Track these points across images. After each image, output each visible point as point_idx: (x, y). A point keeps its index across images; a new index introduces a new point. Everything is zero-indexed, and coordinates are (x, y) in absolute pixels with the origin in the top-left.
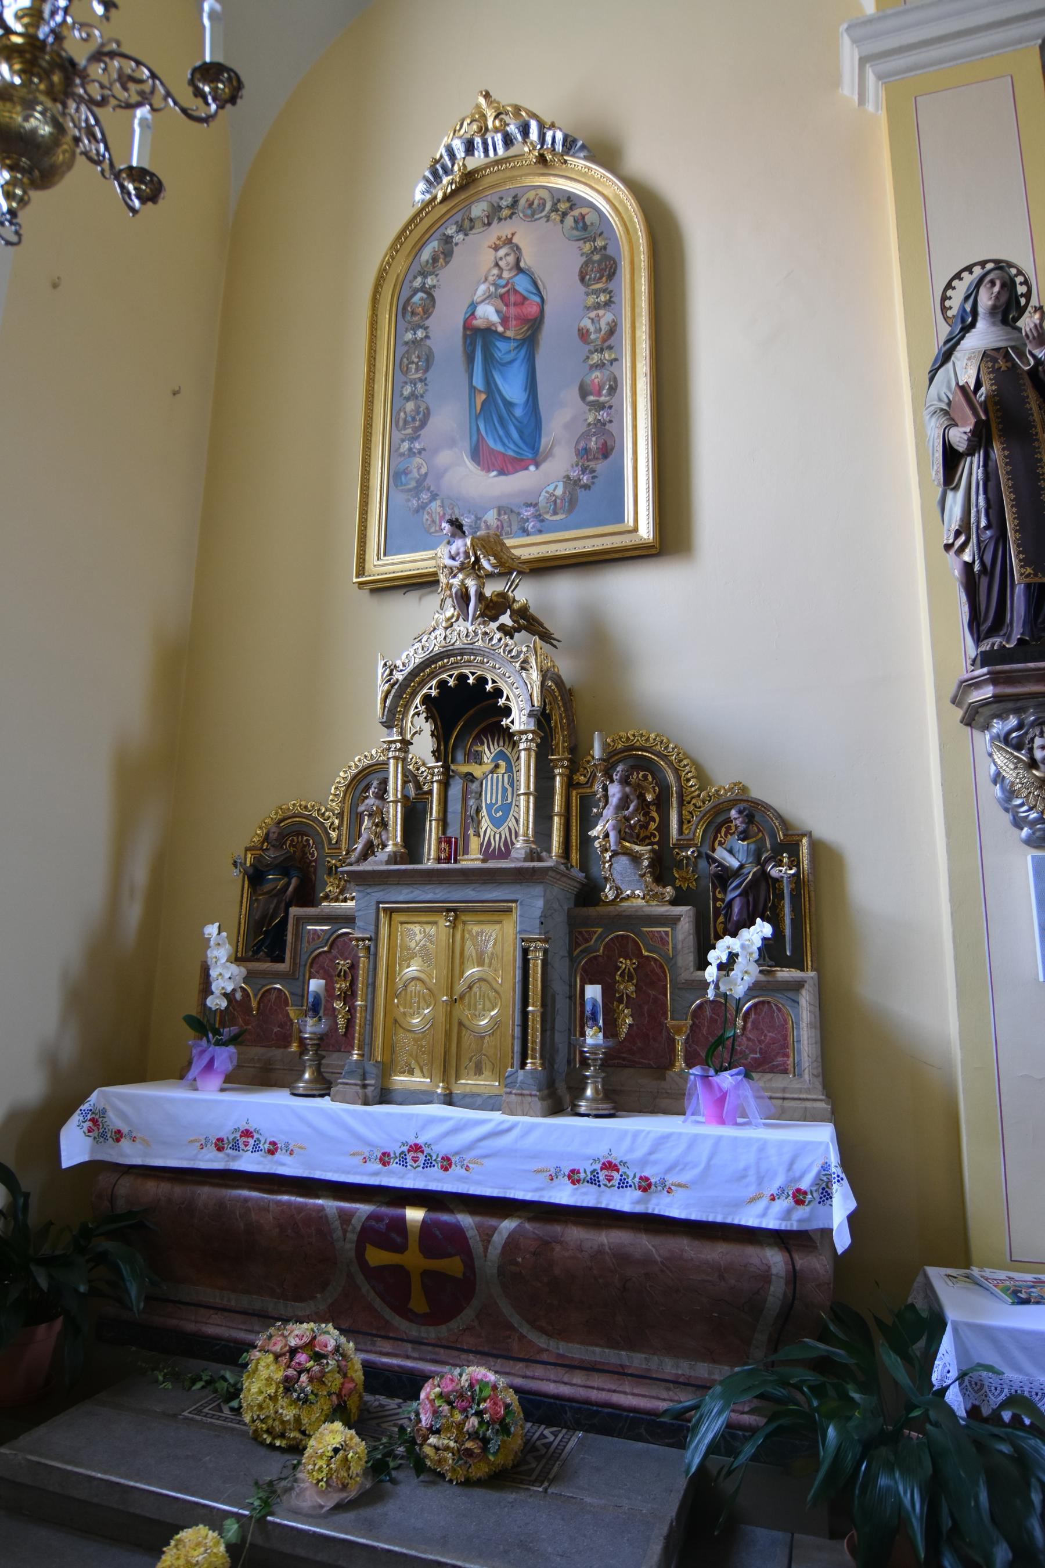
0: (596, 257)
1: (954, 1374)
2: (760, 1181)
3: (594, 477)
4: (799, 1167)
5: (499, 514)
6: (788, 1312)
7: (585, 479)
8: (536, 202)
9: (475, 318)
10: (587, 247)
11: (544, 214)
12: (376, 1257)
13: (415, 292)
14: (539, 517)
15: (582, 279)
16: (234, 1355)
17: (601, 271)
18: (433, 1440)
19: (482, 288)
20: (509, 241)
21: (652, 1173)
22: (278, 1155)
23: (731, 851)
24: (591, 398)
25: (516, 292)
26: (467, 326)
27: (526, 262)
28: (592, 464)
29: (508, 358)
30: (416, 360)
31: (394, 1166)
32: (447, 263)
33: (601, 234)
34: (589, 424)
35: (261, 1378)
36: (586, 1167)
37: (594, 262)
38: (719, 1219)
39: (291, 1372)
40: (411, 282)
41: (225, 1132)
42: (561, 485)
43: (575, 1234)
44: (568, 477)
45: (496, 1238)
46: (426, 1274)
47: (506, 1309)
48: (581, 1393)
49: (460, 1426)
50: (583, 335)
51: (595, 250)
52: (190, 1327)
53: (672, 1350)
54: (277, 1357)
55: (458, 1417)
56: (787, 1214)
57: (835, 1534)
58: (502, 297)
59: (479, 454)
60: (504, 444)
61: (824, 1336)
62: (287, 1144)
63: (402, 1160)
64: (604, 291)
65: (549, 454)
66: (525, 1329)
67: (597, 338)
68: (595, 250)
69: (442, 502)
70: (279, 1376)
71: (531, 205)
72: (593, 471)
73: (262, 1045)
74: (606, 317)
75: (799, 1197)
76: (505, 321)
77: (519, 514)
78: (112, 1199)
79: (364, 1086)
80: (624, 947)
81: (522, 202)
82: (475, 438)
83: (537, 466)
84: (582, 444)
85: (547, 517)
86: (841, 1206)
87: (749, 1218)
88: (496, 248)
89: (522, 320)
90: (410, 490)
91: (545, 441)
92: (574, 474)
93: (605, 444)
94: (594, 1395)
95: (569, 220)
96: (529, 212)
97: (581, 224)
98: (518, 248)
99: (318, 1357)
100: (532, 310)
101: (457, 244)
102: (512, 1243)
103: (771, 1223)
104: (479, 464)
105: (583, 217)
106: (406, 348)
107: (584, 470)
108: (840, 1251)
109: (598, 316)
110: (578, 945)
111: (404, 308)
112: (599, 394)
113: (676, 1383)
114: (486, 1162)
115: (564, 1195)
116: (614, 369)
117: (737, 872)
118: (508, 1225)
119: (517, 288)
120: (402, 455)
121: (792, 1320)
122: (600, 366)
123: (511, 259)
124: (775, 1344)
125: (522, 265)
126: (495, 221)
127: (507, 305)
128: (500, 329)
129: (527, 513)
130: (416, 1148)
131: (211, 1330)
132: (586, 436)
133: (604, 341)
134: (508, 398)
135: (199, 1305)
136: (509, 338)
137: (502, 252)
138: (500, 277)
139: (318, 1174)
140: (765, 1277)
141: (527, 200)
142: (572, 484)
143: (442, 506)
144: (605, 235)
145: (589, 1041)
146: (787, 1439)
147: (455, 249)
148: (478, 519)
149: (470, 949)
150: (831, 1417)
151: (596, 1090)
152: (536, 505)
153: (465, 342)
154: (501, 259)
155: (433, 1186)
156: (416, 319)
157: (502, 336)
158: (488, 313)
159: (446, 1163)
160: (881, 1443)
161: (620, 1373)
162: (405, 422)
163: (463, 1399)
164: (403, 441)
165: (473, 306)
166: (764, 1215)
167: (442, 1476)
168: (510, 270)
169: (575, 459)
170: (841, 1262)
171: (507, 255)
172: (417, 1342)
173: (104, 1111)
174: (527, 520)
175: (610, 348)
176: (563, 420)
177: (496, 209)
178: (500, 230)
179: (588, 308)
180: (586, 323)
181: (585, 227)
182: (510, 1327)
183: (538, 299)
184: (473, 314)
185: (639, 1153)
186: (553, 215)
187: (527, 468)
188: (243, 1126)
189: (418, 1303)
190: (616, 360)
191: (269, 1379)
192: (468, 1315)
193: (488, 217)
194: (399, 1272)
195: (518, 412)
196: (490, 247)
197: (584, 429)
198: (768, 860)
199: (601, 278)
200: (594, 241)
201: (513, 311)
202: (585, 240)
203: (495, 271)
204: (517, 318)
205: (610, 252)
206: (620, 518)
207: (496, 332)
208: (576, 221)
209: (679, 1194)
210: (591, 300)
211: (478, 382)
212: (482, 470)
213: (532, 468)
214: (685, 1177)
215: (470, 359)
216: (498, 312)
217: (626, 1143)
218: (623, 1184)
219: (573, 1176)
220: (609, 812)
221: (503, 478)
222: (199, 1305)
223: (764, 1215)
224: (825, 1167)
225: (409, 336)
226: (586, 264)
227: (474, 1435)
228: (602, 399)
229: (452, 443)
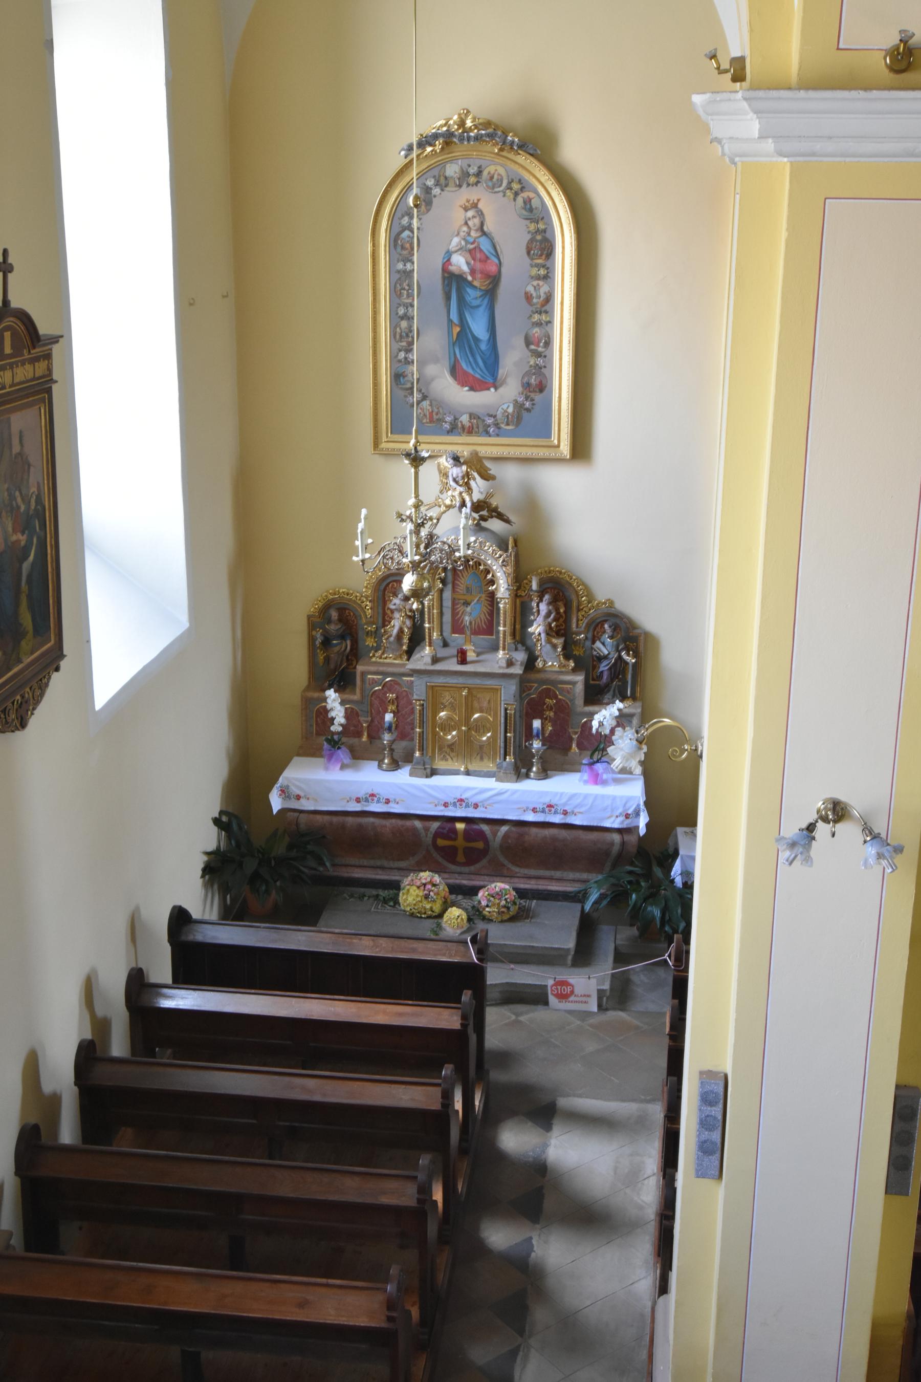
0: (539, 237)
1: (679, 872)
2: (612, 810)
3: (533, 404)
4: (628, 805)
5: (470, 418)
6: (620, 855)
7: (527, 404)
8: (496, 177)
9: (451, 264)
10: (532, 227)
11: (501, 189)
12: (441, 842)
13: (404, 229)
14: (497, 425)
15: (528, 253)
16: (396, 886)
17: (542, 250)
18: (487, 909)
19: (456, 240)
20: (475, 206)
21: (567, 808)
22: (391, 804)
23: (603, 644)
24: (533, 347)
25: (481, 250)
26: (445, 269)
27: (489, 226)
28: (532, 395)
29: (477, 302)
30: (407, 288)
31: (450, 807)
32: (428, 211)
33: (543, 218)
34: (531, 366)
35: (410, 897)
36: (540, 807)
37: (537, 241)
38: (595, 824)
39: (426, 892)
40: (400, 219)
41: (361, 794)
42: (511, 406)
43: (534, 830)
44: (516, 401)
45: (499, 834)
46: (465, 848)
47: (502, 859)
48: (535, 887)
49: (499, 904)
50: (528, 297)
51: (538, 231)
52: (346, 875)
53: (572, 869)
54: (418, 887)
55: (497, 901)
56: (622, 822)
57: (632, 925)
58: (470, 251)
59: (455, 371)
60: (473, 369)
61: (632, 864)
62: (395, 800)
63: (455, 804)
64: (544, 266)
65: (504, 382)
66: (510, 866)
67: (538, 303)
68: (538, 231)
69: (431, 402)
70: (421, 894)
71: (492, 178)
72: (532, 400)
73: (357, 742)
74: (544, 289)
75: (627, 816)
76: (473, 272)
77: (484, 421)
78: (297, 824)
79: (425, 769)
80: (549, 693)
81: (485, 173)
82: (453, 359)
83: (496, 389)
84: (526, 379)
85: (503, 426)
86: (643, 821)
87: (607, 824)
88: (466, 209)
89: (487, 275)
90: (407, 389)
91: (501, 372)
92: (521, 399)
93: (541, 382)
94: (540, 887)
95: (520, 200)
96: (490, 184)
97: (528, 206)
98: (482, 214)
99: (434, 885)
100: (493, 269)
101: (435, 196)
102: (506, 836)
103: (616, 826)
104: (456, 380)
105: (530, 200)
106: (398, 276)
107: (527, 398)
108: (641, 835)
109: (538, 285)
110: (524, 692)
111: (396, 241)
112: (538, 346)
113: (578, 881)
114: (495, 805)
115: (530, 817)
116: (548, 328)
117: (606, 657)
118: (504, 829)
119: (482, 247)
120: (400, 361)
121: (621, 858)
122: (539, 324)
123: (477, 221)
124: (614, 866)
125: (485, 229)
126: (465, 186)
127: (474, 259)
128: (470, 278)
129: (490, 421)
130: (461, 800)
131: (356, 875)
132: (528, 374)
133: (543, 306)
134: (475, 334)
135: (351, 866)
136: (475, 287)
137: (470, 214)
138: (469, 234)
139: (412, 812)
140: (612, 844)
141: (489, 173)
142: (519, 406)
143: (431, 405)
144: (545, 220)
145: (535, 746)
146: (617, 897)
147: (434, 200)
148: (456, 419)
149: (476, 705)
150: (635, 891)
151: (538, 769)
152: (495, 416)
153: (444, 281)
154: (469, 219)
155: (470, 815)
156: (405, 252)
157: (470, 284)
158: (460, 263)
159: (476, 806)
160: (652, 897)
161: (551, 879)
162: (401, 336)
163: (499, 895)
164: (400, 351)
165: (449, 254)
166: (613, 822)
167: (492, 920)
168: (477, 230)
169: (521, 389)
170: (641, 839)
171: (474, 217)
172: (460, 873)
173: (288, 787)
174: (489, 426)
175: (546, 312)
176: (514, 359)
177: (465, 175)
178: (467, 194)
179: (532, 278)
180: (530, 289)
181: (531, 210)
182: (504, 865)
183: (496, 261)
184: (449, 260)
185: (564, 800)
186: (508, 193)
187: (488, 389)
188: (370, 792)
189: (461, 858)
190: (550, 322)
191: (417, 896)
192: (484, 862)
193: (459, 179)
194: (454, 849)
195: (483, 347)
196: (461, 206)
197: (527, 369)
198: (623, 649)
199: (541, 255)
200: (537, 223)
201: (478, 266)
202: (532, 220)
203: (465, 229)
204: (481, 273)
205: (548, 235)
206: (549, 436)
207: (466, 279)
208: (525, 202)
209: (579, 816)
210: (534, 271)
211: (454, 317)
212: (459, 384)
213: (492, 390)
214: (582, 810)
215: (448, 298)
216: (468, 263)
217: (557, 798)
218: (556, 812)
219: (534, 810)
220: (540, 619)
221: (472, 393)
222: (351, 866)
223: (613, 822)
224: (638, 805)
225: (400, 266)
226: (532, 240)
227: (504, 907)
228: (540, 349)
229: (436, 361)
